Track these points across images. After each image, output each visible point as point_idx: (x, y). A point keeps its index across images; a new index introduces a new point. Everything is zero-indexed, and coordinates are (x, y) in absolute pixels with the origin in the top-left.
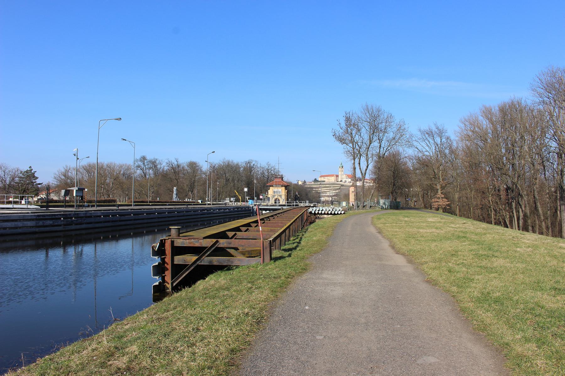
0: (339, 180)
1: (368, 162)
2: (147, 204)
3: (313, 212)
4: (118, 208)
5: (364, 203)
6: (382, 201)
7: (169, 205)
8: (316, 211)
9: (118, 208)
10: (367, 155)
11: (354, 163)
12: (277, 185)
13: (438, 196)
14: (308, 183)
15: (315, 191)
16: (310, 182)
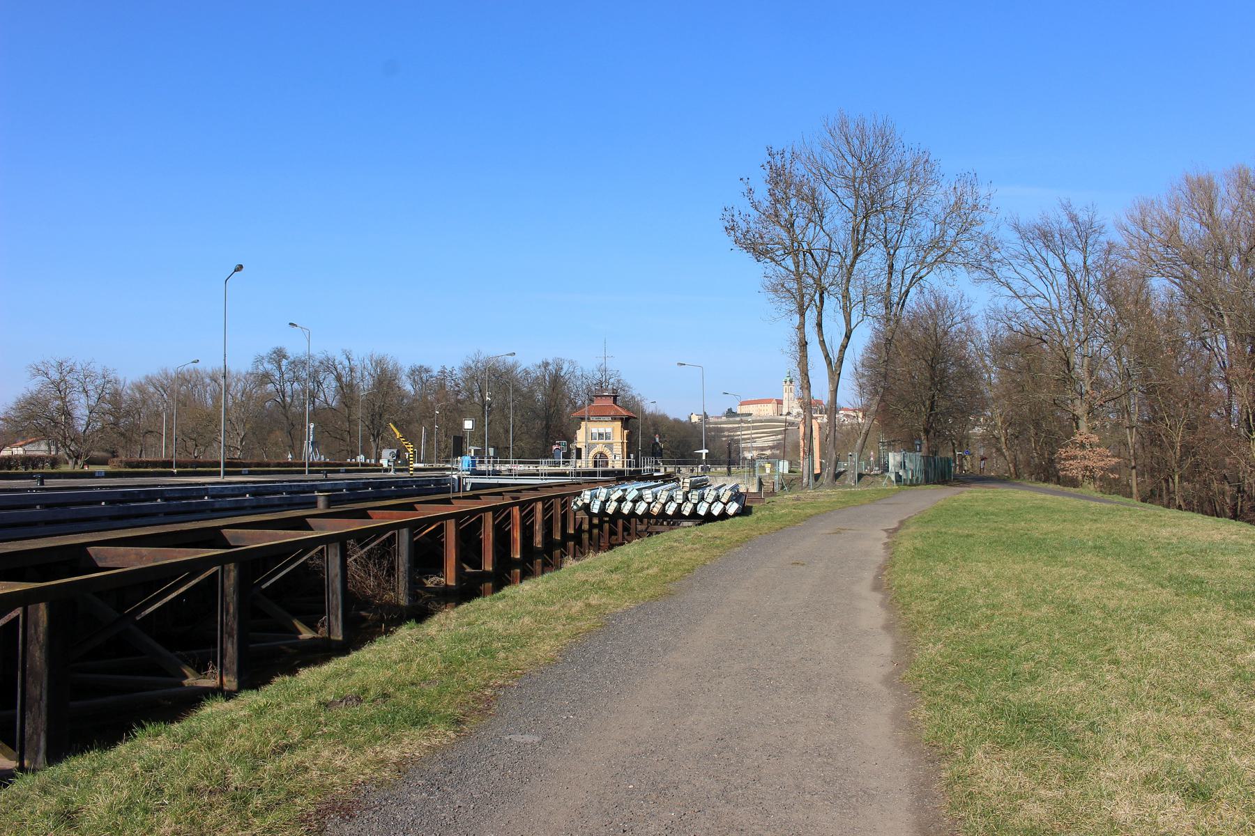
0: (785, 412)
1: (848, 322)
2: (357, 468)
3: (595, 509)
4: (42, 484)
5: (836, 464)
6: (893, 459)
7: (251, 473)
8: (607, 501)
9: (42, 484)
10: (846, 296)
11: (802, 327)
12: (600, 416)
13: (1078, 438)
14: (712, 420)
15: (728, 436)
16: (718, 417)
